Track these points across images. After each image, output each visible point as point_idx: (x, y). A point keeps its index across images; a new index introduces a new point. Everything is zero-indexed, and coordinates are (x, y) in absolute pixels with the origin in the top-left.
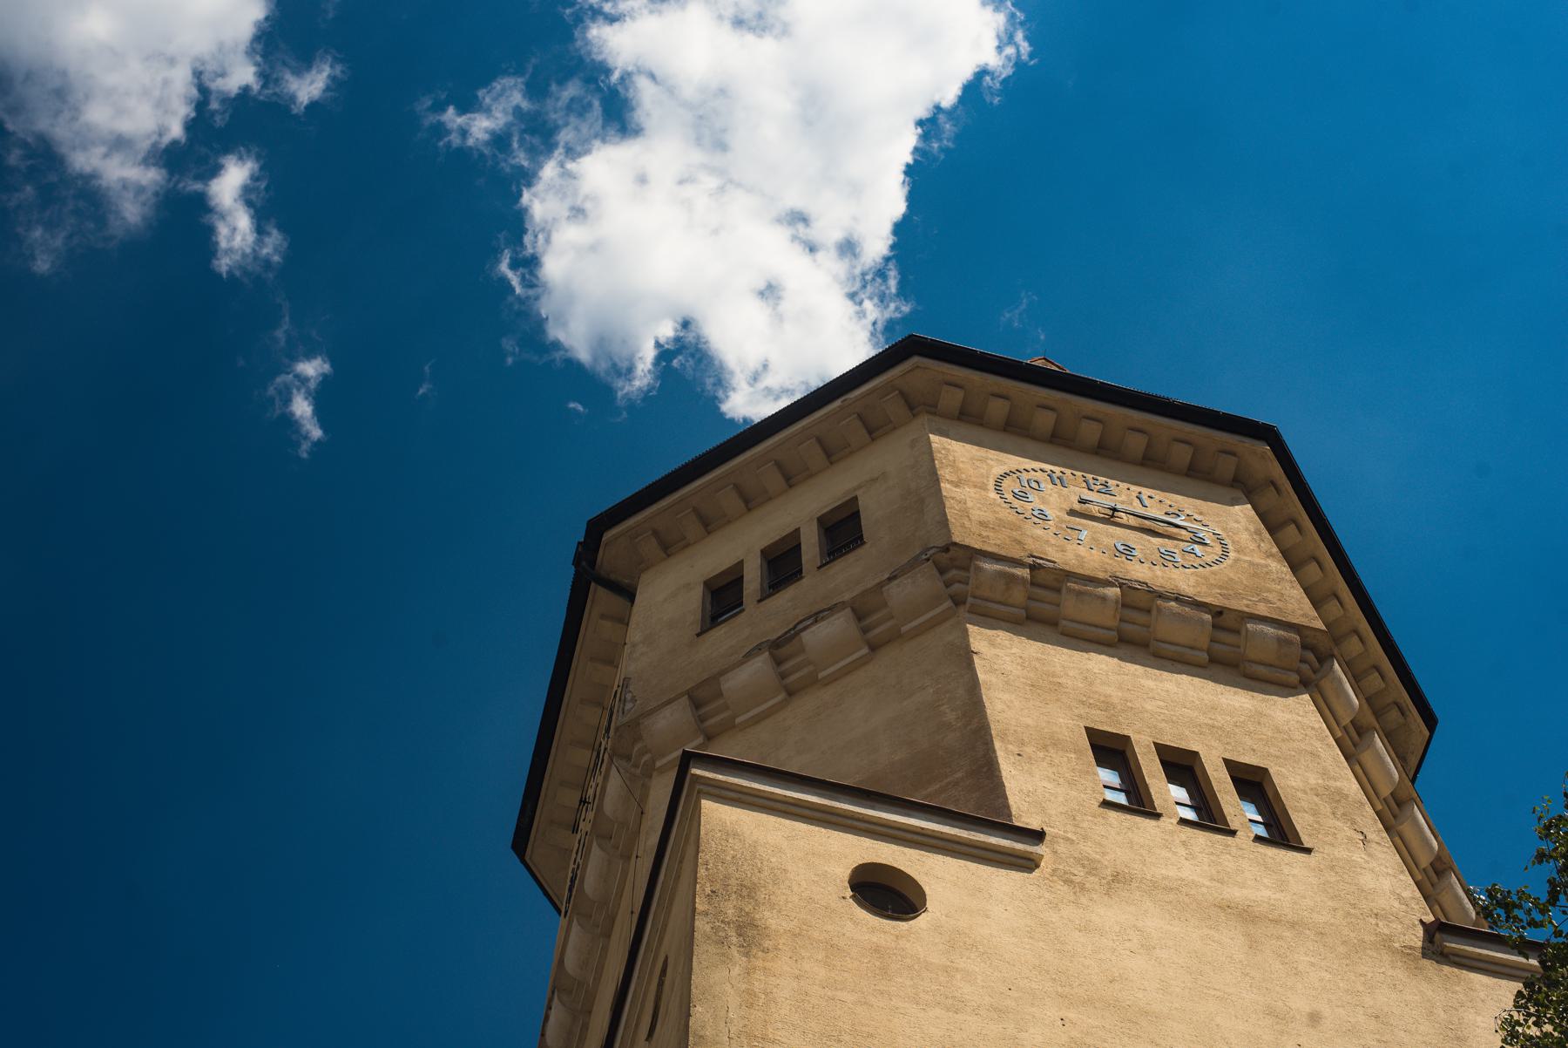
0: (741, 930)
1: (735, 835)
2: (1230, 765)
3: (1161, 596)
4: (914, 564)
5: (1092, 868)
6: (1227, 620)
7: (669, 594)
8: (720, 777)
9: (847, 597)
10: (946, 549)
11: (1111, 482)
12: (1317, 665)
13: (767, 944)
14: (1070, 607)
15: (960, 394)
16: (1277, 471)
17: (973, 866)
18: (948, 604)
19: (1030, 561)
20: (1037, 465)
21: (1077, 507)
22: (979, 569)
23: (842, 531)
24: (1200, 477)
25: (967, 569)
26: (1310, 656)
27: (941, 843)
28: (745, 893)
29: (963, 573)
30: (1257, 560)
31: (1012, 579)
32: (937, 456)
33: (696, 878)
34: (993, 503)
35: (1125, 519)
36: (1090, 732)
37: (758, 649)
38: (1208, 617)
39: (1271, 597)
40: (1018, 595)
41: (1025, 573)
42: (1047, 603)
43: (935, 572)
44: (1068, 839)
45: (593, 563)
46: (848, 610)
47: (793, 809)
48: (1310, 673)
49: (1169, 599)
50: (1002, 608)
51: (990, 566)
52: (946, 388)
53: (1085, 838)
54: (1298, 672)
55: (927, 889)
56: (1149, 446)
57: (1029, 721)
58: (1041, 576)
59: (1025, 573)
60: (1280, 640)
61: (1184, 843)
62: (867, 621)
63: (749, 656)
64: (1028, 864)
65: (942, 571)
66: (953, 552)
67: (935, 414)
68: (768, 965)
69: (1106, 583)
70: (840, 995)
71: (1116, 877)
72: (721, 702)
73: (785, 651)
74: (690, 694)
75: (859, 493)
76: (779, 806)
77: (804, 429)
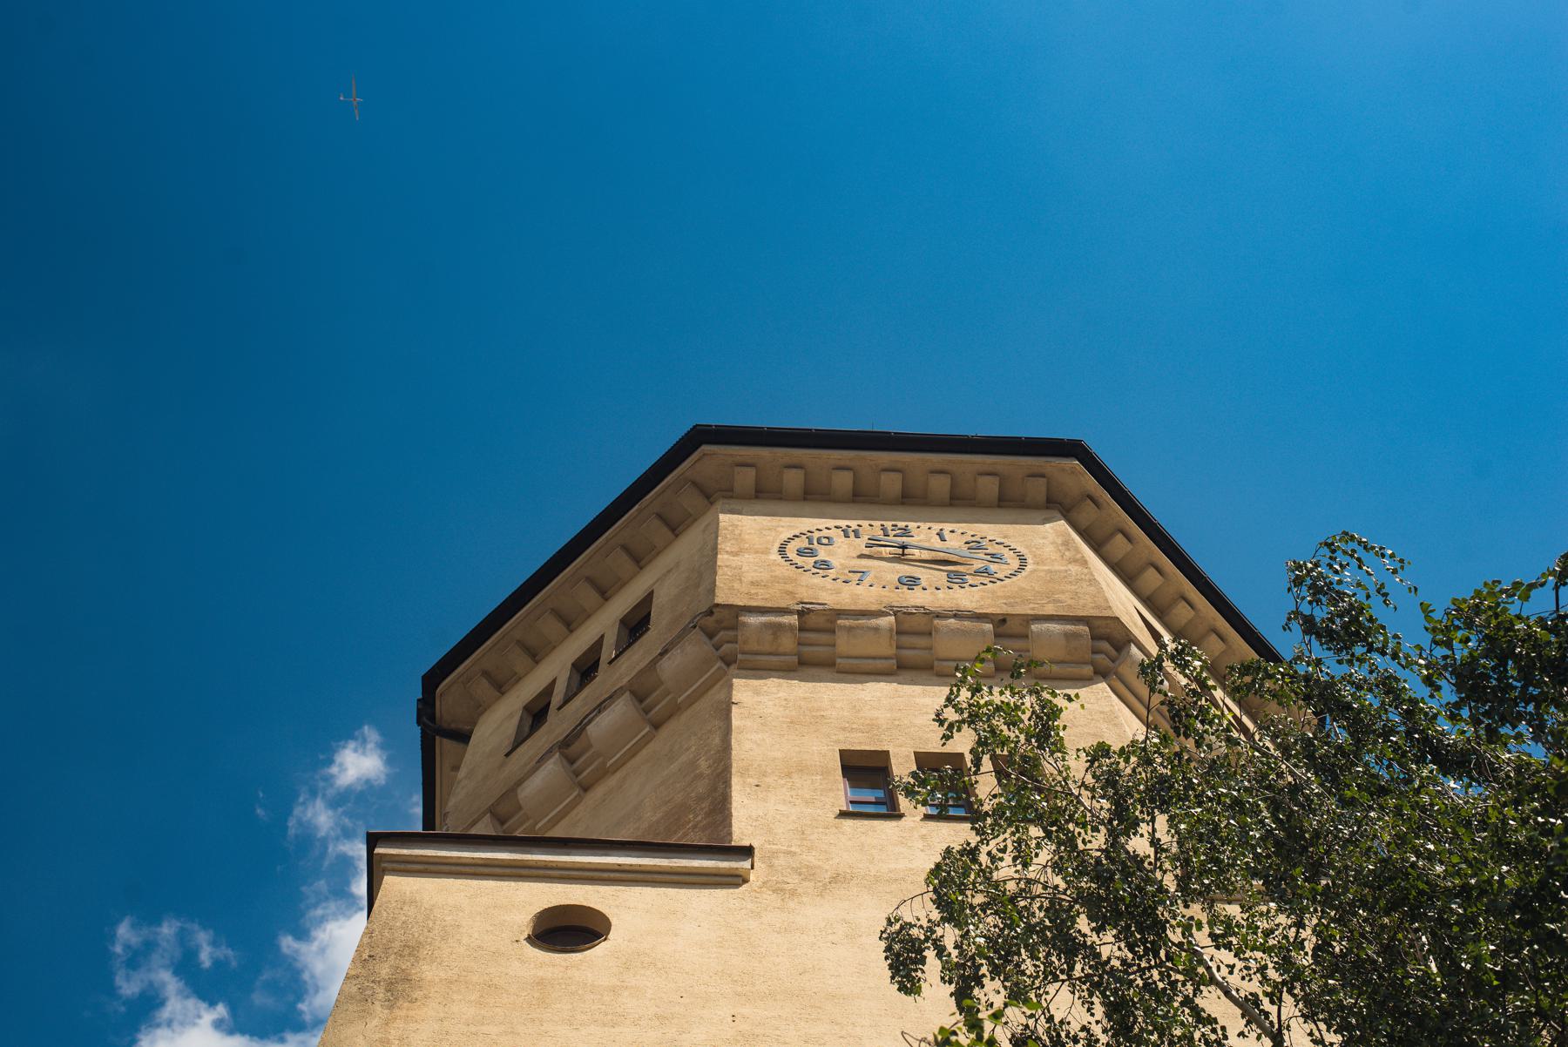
0: (390, 986)
1: (413, 902)
2: (648, 599)
3: (938, 616)
4: (685, 632)
5: (807, 873)
6: (1012, 627)
7: (496, 725)
8: (405, 852)
10: (710, 613)
11: (912, 525)
12: (1114, 653)
13: (417, 994)
14: (844, 644)
15: (752, 472)
16: (1091, 483)
17: (671, 892)
18: (719, 664)
19: (799, 607)
20: (831, 523)
21: (867, 551)
22: (744, 624)
23: (636, 625)
24: (1011, 503)
25: (734, 627)
26: (1106, 646)
27: (640, 876)
28: (407, 952)
29: (731, 633)
30: (1057, 567)
31: (778, 628)
32: (722, 532)
34: (774, 563)
35: (917, 553)
37: (550, 752)
38: (989, 627)
39: (1062, 597)
40: (787, 643)
41: (793, 620)
42: (815, 645)
43: (704, 638)
44: (789, 853)
45: (432, 718)
48: (1107, 662)
49: (946, 617)
50: (774, 658)
51: (753, 620)
52: (738, 469)
53: (810, 849)
54: (1092, 663)
55: (614, 921)
56: (953, 486)
57: (779, 755)
58: (812, 620)
59: (793, 620)
60: (1069, 636)
61: (923, 837)
62: (648, 701)
64: (735, 880)
65: (711, 636)
66: (718, 614)
68: (411, 1013)
70: (485, 1029)
71: (835, 879)
73: (575, 748)
76: (467, 869)
77: (608, 540)
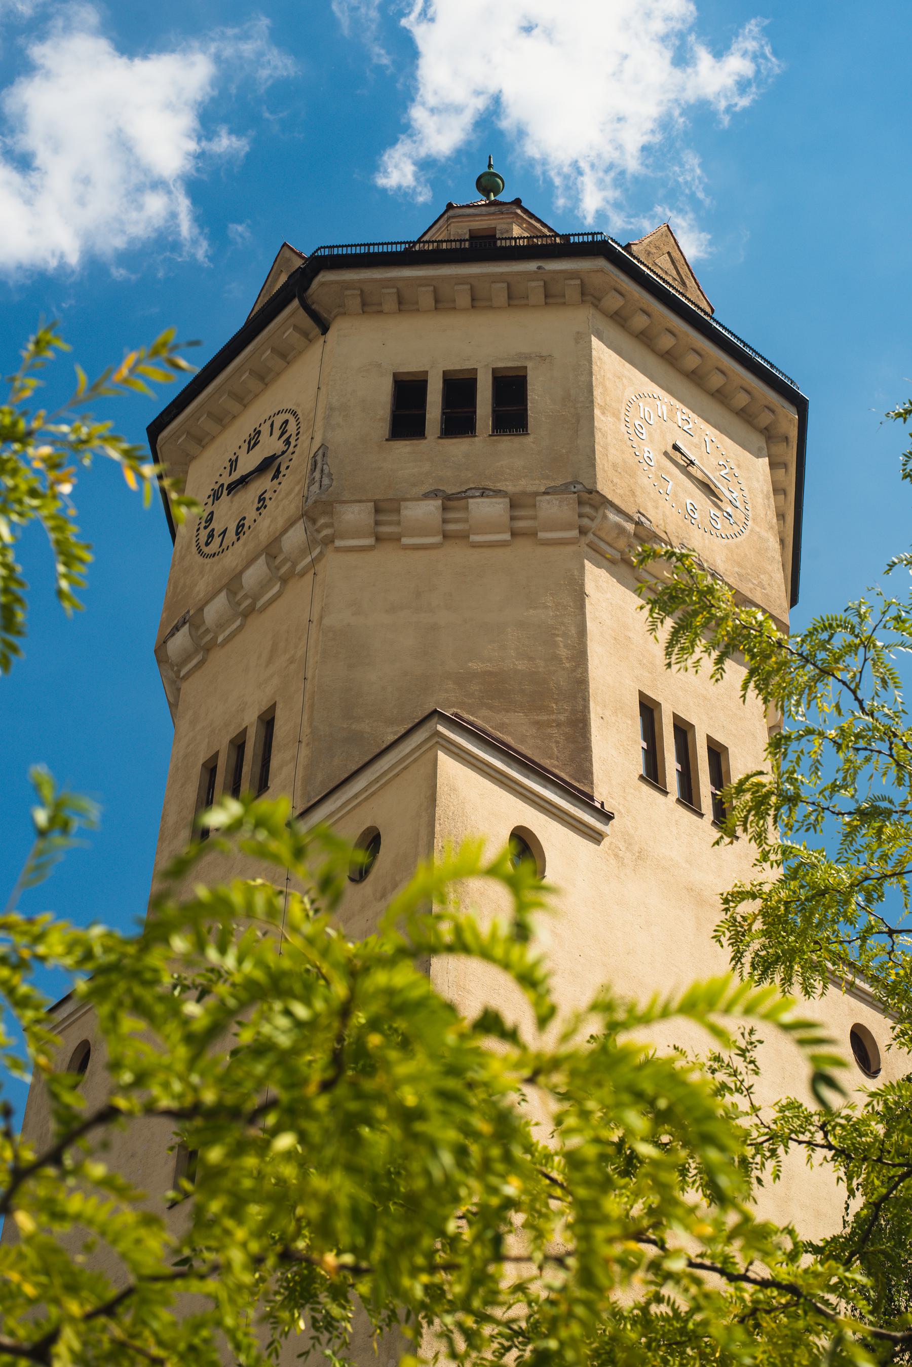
9: (510, 488)
16: (794, 433)
22: (605, 517)
31: (622, 530)
33: (434, 833)
36: (641, 694)
46: (507, 500)
47: (485, 768)
51: (613, 517)
64: (596, 837)
66: (594, 495)
72: (394, 518)
74: (376, 502)
75: (530, 365)
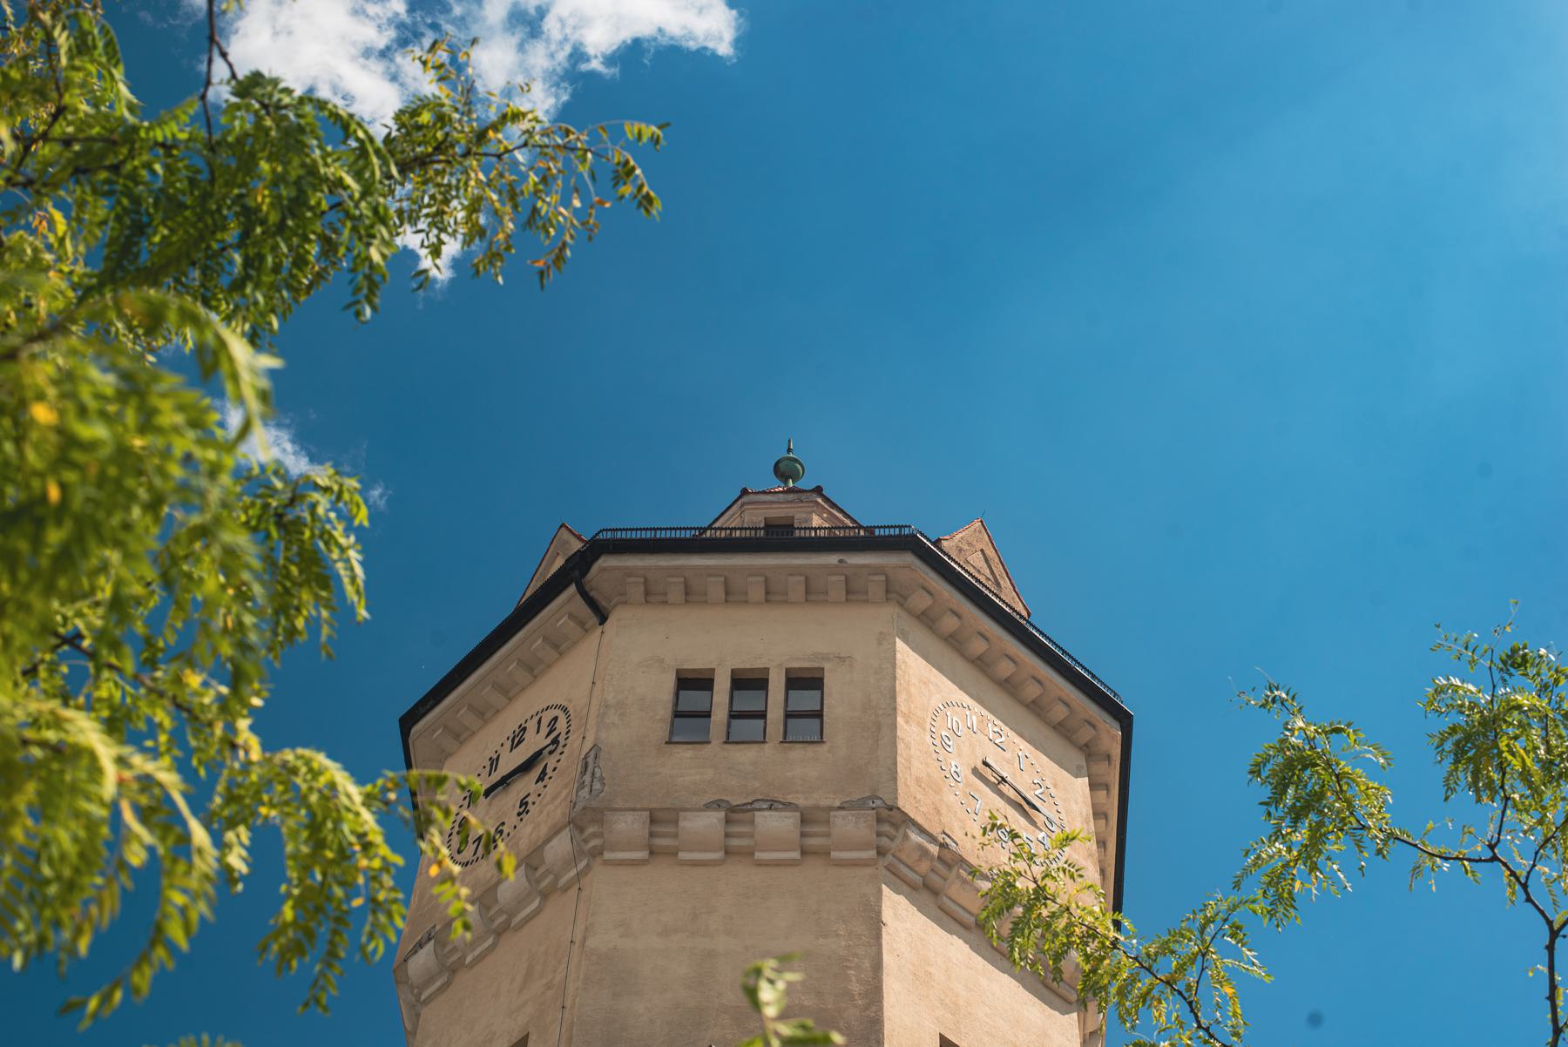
9: (802, 801)
10: (891, 809)
16: (1116, 752)
22: (906, 837)
37: (717, 805)
40: (924, 867)
51: (915, 837)
63: (708, 807)
66: (894, 812)
67: (902, 605)
69: (985, 877)
72: (670, 829)
74: (651, 811)
75: (827, 666)
